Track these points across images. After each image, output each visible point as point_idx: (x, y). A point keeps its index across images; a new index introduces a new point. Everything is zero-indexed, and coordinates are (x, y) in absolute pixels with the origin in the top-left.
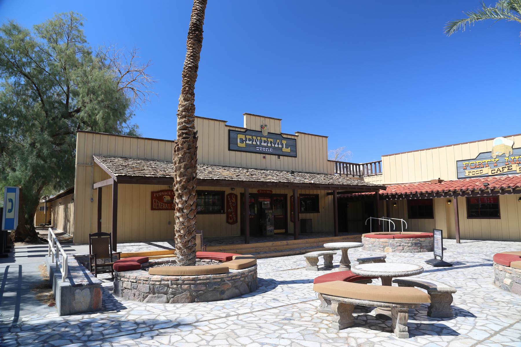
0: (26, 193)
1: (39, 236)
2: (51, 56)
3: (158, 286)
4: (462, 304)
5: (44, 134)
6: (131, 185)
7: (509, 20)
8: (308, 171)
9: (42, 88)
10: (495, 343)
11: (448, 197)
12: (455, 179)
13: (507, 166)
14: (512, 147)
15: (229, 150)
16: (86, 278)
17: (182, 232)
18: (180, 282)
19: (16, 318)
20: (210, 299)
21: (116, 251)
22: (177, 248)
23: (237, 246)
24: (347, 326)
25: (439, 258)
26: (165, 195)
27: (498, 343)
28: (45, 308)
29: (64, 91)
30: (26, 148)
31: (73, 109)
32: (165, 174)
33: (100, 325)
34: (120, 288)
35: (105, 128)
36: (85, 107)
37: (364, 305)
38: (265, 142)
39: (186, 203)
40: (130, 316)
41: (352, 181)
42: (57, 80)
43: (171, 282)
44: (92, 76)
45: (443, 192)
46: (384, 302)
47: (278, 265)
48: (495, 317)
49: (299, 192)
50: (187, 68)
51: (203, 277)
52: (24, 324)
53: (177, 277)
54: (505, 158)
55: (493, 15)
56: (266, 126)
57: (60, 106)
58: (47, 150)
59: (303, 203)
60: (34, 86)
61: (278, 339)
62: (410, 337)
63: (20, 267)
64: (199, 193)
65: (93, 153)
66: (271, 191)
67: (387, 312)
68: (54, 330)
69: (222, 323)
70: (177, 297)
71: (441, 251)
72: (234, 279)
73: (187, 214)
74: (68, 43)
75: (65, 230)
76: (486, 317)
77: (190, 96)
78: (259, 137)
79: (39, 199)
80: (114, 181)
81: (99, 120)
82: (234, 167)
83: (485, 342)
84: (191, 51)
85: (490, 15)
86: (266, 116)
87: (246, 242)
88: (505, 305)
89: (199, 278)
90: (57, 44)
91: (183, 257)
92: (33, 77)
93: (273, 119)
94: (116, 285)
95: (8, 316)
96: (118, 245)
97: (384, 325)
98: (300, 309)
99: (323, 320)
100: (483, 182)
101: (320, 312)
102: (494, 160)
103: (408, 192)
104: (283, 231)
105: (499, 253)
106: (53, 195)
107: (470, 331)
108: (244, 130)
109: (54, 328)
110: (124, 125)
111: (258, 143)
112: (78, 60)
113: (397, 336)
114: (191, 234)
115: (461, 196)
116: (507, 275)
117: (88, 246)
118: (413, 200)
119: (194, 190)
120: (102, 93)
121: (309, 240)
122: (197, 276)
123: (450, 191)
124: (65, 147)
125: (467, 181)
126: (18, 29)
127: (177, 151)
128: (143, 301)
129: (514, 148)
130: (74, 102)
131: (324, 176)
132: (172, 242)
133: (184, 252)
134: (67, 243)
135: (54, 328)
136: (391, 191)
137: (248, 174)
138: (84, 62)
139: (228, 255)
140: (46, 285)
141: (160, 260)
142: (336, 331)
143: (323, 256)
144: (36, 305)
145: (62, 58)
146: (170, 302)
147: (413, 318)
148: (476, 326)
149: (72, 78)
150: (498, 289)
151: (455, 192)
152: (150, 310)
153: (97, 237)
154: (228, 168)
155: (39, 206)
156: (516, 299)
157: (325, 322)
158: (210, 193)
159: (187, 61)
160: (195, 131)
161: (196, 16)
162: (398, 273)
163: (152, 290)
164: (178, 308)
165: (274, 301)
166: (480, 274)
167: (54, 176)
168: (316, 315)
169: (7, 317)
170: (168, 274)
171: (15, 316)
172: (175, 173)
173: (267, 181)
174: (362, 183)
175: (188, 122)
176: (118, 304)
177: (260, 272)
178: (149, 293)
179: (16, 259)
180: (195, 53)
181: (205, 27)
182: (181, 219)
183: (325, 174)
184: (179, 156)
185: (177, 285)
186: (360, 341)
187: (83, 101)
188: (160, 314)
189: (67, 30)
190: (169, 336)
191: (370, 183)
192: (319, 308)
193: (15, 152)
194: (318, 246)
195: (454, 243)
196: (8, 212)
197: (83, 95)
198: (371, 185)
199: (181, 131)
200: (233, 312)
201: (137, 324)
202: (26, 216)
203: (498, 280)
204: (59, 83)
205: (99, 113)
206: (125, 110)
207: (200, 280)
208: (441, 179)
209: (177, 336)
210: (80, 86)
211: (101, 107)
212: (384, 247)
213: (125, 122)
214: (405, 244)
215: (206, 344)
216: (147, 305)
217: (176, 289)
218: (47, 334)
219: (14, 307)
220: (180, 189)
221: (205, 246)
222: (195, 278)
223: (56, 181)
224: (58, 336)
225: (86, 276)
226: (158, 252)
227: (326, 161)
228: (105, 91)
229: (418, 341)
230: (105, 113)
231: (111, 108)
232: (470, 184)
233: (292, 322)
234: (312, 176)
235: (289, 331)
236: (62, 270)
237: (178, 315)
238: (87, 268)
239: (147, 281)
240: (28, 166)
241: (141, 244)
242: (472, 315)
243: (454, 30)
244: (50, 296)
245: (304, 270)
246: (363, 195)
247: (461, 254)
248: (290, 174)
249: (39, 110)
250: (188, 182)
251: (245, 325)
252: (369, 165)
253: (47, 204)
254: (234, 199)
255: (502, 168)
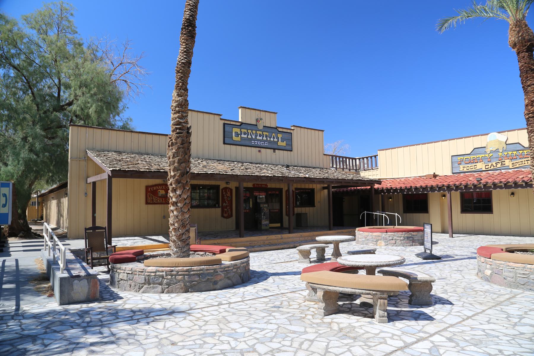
0: (19, 188)
1: (32, 231)
2: (41, 47)
3: (153, 277)
4: (443, 293)
5: (36, 128)
6: (125, 179)
7: (498, 18)
8: (303, 165)
9: (33, 80)
10: (465, 326)
11: (442, 191)
12: (449, 173)
13: (500, 161)
14: (506, 143)
15: (224, 143)
16: (83, 270)
17: (176, 225)
18: (174, 273)
19: (17, 307)
20: (203, 289)
21: (111, 245)
22: (172, 241)
23: (231, 239)
24: (332, 313)
25: (428, 252)
26: (160, 189)
27: (468, 326)
28: (44, 299)
29: (55, 84)
30: (18, 142)
31: (65, 102)
32: (159, 168)
33: (98, 313)
34: (116, 280)
35: (98, 122)
36: (78, 100)
37: (347, 292)
38: (260, 136)
39: (180, 197)
40: (126, 305)
41: (348, 175)
42: (48, 73)
43: (166, 273)
44: (84, 69)
45: (437, 187)
46: (365, 290)
47: (271, 258)
48: (471, 304)
49: (295, 186)
50: (180, 63)
51: (197, 268)
52: (25, 313)
53: (172, 268)
54: (499, 154)
55: (483, 13)
56: (261, 119)
57: (51, 99)
58: (40, 144)
59: (299, 197)
60: (23, 78)
61: (266, 324)
62: (389, 322)
63: (17, 261)
64: (194, 187)
65: (87, 147)
66: (266, 185)
67: (370, 300)
68: (55, 318)
69: (214, 310)
70: (172, 287)
71: (431, 244)
72: (226, 270)
73: (181, 208)
74: (58, 34)
75: (58, 225)
76: (463, 304)
77: (184, 92)
78: (254, 130)
79: (31, 194)
80: (109, 175)
81: (92, 114)
82: (229, 161)
83: (456, 325)
84: (185, 46)
85: (480, 14)
86: (261, 110)
87: (241, 236)
88: (482, 294)
89: (193, 270)
90: (46, 35)
91: (177, 250)
92: (23, 69)
93: (269, 112)
94: (112, 277)
95: (10, 306)
96: (113, 239)
97: (366, 312)
98: (289, 298)
99: (310, 308)
100: (476, 177)
101: (308, 301)
102: (488, 155)
103: (403, 186)
104: (279, 225)
105: (483, 246)
106: (45, 190)
107: (445, 316)
108: (239, 124)
109: (54, 316)
110: (117, 118)
111: (254, 137)
112: (69, 52)
113: (377, 321)
114: (185, 227)
115: (455, 190)
116: (488, 266)
117: (84, 241)
118: (408, 195)
119: (188, 184)
120: (94, 86)
121: (304, 234)
122: (190, 267)
123: (443, 185)
124: (57, 141)
125: (462, 176)
126: (4, 19)
127: (171, 146)
128: (139, 291)
129: (507, 143)
130: (66, 95)
131: (319, 170)
132: (166, 236)
133: (178, 244)
134: (63, 237)
135: (54, 316)
136: (385, 185)
137: (242, 168)
138: (75, 54)
139: (222, 247)
140: (44, 277)
141: (155, 253)
142: (321, 317)
143: (315, 250)
144: (35, 296)
145: (53, 49)
146: (165, 292)
147: (394, 306)
148: (451, 312)
149: (64, 71)
150: (480, 280)
151: (449, 188)
152: (146, 300)
153: (92, 231)
154: (223, 162)
155: (30, 200)
156: (494, 288)
157: (312, 309)
158: (204, 187)
159: (180, 57)
160: (189, 126)
161: (189, 11)
162: (380, 263)
163: (147, 281)
164: (172, 298)
165: (265, 291)
166: (466, 267)
167: (46, 171)
168: (304, 304)
169: (8, 306)
170: (162, 266)
171: (16, 306)
172: (169, 168)
173: (261, 175)
174: (358, 177)
175: (181, 117)
176: (115, 294)
177: (254, 264)
178: (145, 284)
179: (11, 253)
180: (188, 49)
181: (198, 23)
182: (175, 213)
183: (321, 168)
184: (172, 151)
185: (172, 275)
186: (341, 326)
187: (76, 94)
188: (155, 303)
189: (57, 20)
190: (164, 323)
191: (366, 177)
192: (307, 297)
193: (7, 146)
194: (312, 240)
195: (447, 238)
196: (2, 207)
197: (75, 88)
198: (366, 180)
199: (174, 127)
200: (226, 301)
201: (133, 312)
202: (19, 211)
203: (480, 271)
204: (50, 75)
205: (91, 106)
206: (119, 104)
207: (194, 271)
208: (436, 174)
209: (172, 322)
210: (72, 78)
211: (93, 100)
212: (377, 241)
213: (118, 115)
214: (397, 238)
215: (199, 328)
216: (142, 295)
217: (171, 280)
218: (49, 321)
219: (14, 298)
220: (174, 183)
221: (200, 239)
222: (188, 269)
223: (49, 175)
224: (58, 323)
225: (83, 267)
226: (153, 245)
227: (321, 155)
228: (98, 84)
229: (396, 326)
230: (98, 107)
231: (104, 101)
232: (464, 179)
233: (281, 309)
234: (307, 170)
235: (277, 317)
236: (60, 262)
237: (173, 304)
238: (83, 260)
239: (142, 272)
240: (20, 161)
241: (136, 238)
242: (450, 303)
243: (446, 27)
244: (48, 287)
245: (296, 263)
246: (358, 189)
247: (452, 248)
248: (285, 169)
249: (30, 103)
250: (182, 176)
251: (236, 312)
252: (365, 159)
253: (39, 198)
254: (229, 193)
255: (496, 163)
